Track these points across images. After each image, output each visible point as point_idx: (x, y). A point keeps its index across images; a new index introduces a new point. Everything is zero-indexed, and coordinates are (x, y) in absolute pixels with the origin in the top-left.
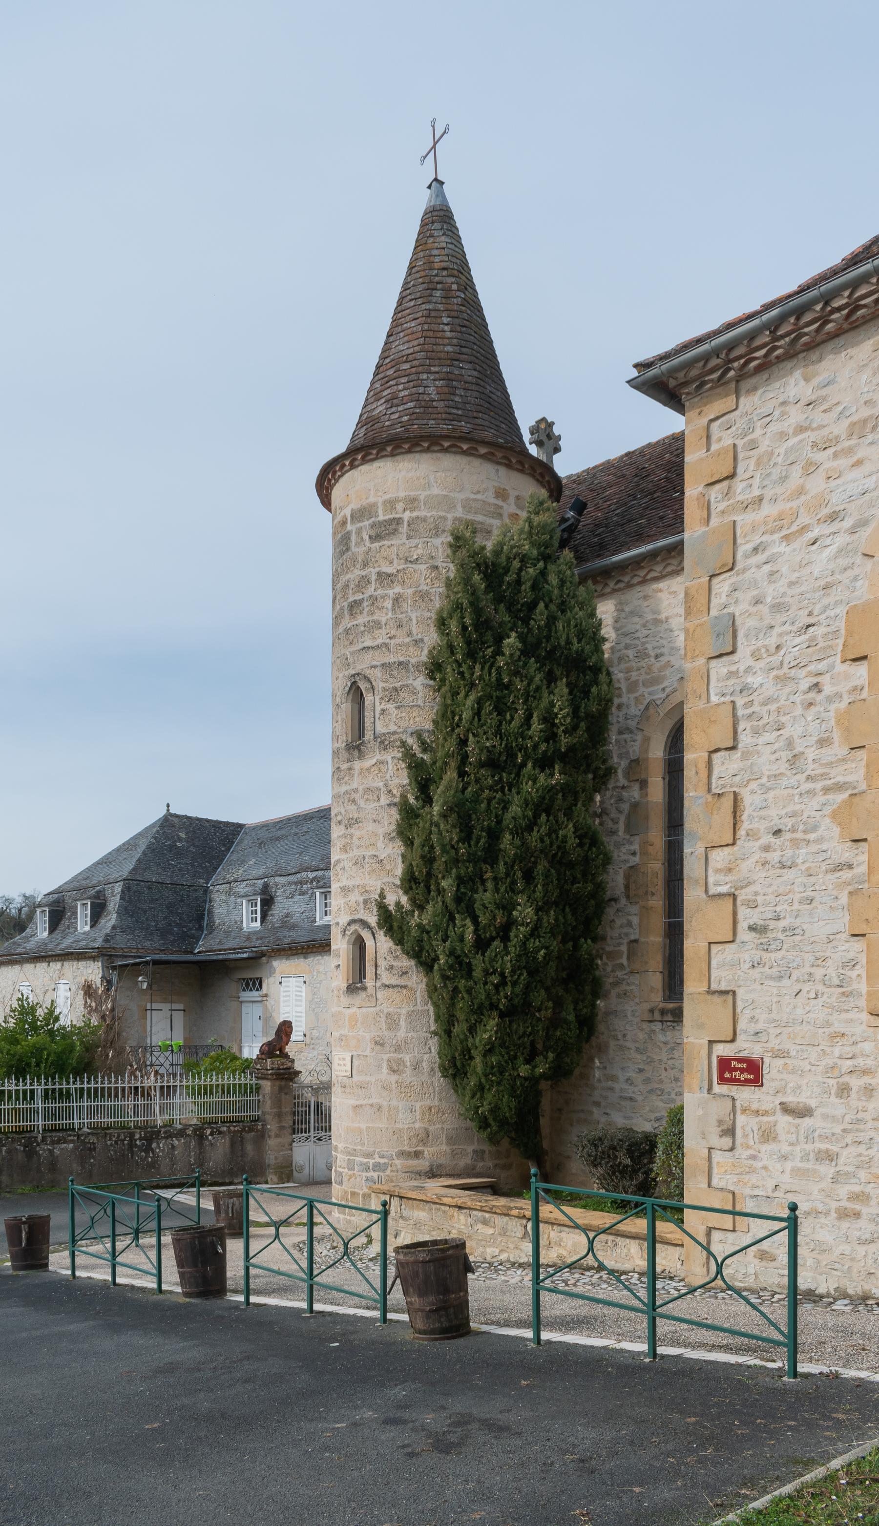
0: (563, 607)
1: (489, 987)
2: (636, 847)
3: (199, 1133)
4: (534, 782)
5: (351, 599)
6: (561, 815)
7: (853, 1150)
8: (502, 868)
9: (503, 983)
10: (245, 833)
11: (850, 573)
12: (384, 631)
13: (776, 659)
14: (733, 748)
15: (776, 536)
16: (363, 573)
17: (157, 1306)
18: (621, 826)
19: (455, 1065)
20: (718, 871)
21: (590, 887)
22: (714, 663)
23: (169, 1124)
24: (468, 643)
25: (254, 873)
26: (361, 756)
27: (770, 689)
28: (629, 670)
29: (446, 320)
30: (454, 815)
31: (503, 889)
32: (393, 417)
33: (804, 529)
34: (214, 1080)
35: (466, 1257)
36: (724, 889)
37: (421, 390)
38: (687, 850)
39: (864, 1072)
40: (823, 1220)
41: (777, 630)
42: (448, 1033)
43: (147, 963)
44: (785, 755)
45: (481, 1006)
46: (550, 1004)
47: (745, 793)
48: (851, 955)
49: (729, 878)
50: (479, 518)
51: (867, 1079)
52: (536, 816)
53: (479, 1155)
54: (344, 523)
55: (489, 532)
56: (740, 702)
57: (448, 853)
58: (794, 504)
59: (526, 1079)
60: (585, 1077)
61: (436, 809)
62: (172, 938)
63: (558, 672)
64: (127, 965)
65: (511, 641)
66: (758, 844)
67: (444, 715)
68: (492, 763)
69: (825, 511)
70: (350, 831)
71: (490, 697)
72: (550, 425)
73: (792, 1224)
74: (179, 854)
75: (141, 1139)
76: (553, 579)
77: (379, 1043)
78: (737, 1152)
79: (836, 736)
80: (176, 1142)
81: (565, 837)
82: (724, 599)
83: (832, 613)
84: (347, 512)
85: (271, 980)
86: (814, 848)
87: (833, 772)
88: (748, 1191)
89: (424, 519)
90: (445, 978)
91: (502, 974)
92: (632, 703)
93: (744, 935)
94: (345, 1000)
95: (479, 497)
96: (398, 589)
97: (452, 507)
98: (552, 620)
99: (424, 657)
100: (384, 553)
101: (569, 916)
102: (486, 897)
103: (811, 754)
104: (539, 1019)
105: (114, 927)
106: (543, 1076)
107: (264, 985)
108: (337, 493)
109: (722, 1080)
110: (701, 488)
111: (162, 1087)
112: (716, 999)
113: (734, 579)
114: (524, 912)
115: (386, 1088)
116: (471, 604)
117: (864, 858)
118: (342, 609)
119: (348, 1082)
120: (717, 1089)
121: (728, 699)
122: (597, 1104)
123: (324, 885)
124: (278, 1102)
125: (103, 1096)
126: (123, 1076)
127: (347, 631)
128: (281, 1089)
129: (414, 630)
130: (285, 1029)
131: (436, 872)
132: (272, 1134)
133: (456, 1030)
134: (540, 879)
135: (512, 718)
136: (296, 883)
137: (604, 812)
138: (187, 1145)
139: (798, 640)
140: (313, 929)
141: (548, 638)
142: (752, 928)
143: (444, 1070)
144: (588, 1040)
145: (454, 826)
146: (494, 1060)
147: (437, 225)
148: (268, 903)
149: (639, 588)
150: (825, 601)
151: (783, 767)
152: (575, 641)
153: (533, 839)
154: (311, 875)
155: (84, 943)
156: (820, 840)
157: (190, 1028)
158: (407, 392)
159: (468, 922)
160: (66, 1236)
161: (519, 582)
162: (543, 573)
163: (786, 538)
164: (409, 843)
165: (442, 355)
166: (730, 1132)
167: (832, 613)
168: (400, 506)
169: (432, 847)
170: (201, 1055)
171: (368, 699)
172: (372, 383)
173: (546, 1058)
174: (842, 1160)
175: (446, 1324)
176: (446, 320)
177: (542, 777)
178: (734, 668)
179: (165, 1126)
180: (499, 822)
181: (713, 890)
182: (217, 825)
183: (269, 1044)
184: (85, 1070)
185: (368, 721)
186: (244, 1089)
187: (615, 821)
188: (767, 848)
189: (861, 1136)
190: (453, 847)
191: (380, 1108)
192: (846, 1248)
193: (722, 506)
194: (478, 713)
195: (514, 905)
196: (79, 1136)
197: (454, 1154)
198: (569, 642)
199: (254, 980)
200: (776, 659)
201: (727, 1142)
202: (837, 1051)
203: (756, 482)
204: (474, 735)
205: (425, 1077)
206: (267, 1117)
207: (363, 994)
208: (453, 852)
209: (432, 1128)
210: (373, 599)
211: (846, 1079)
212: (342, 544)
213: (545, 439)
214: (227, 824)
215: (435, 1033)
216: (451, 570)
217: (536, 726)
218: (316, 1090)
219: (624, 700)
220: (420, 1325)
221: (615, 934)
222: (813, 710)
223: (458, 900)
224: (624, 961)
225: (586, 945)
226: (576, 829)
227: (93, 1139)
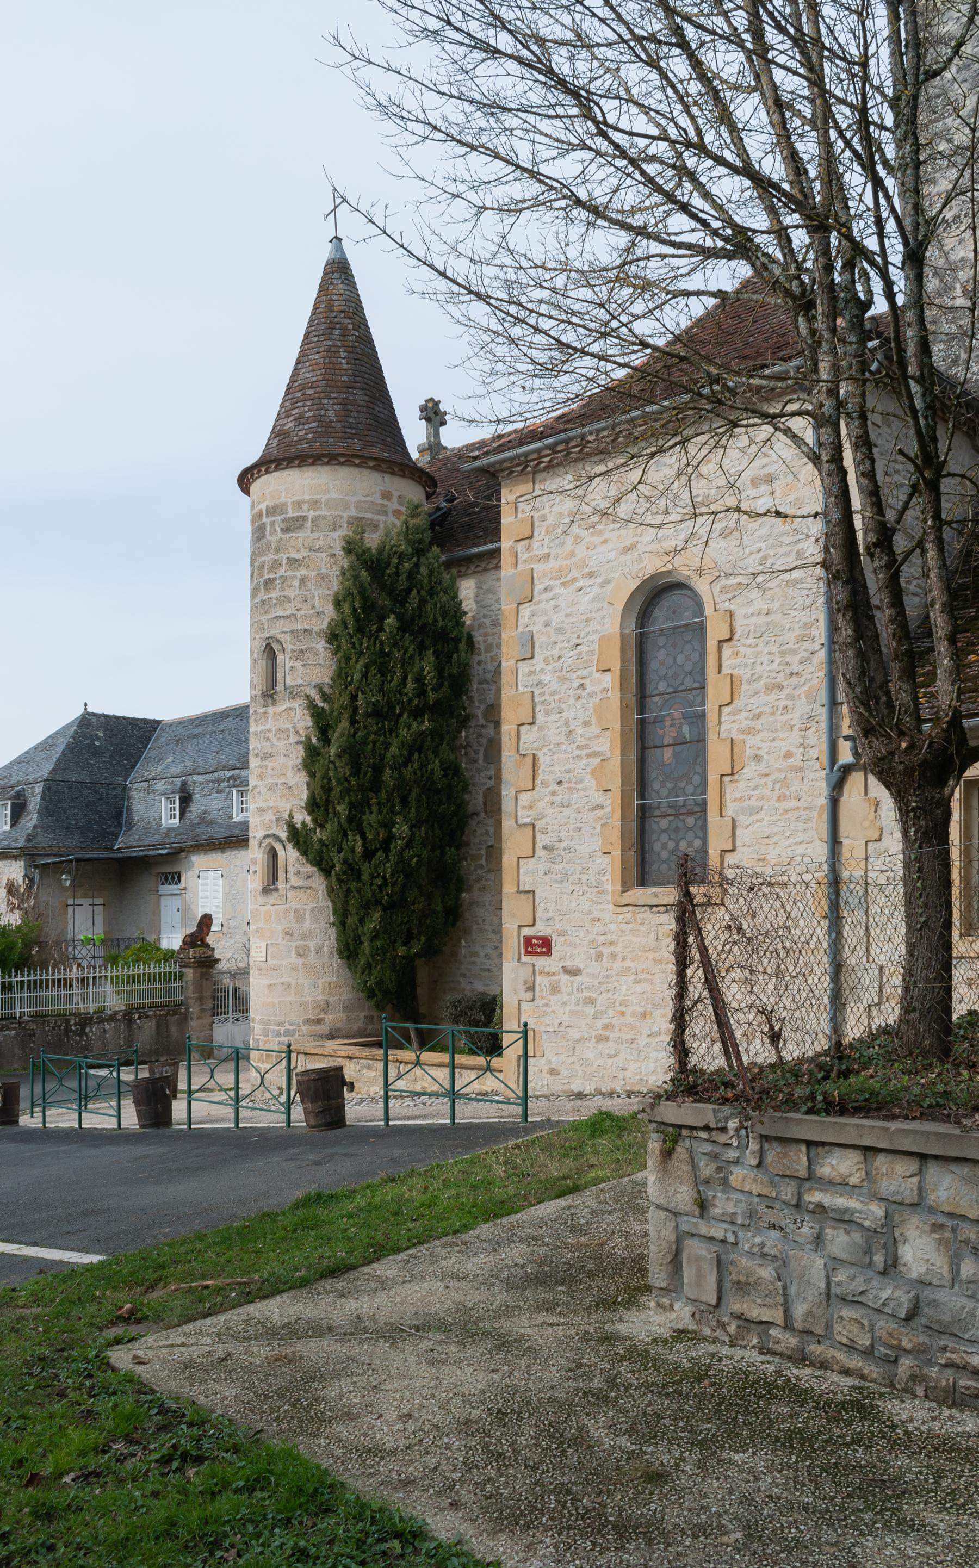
0: (432, 592)
1: (375, 887)
2: (491, 773)
3: (126, 1018)
4: (409, 729)
5: (266, 577)
6: (430, 753)
7: (605, 996)
8: (384, 795)
9: (385, 883)
10: (162, 729)
11: (600, 613)
12: (292, 605)
13: (559, 665)
14: (533, 723)
15: (558, 582)
16: (276, 557)
17: (119, 1136)
18: (481, 756)
19: (349, 949)
20: (524, 808)
21: (453, 808)
22: (520, 664)
23: (101, 1010)
24: (357, 620)
25: (172, 771)
26: (274, 703)
27: (555, 685)
28: (486, 635)
29: (343, 355)
30: (347, 756)
31: (384, 812)
32: (301, 433)
33: (574, 580)
34: (141, 969)
35: (343, 1077)
36: (527, 820)
37: (323, 412)
38: (504, 793)
39: (611, 944)
40: (588, 1044)
41: (559, 645)
42: (343, 924)
43: (70, 861)
44: (564, 730)
45: (368, 902)
46: (422, 899)
47: (540, 755)
48: (603, 866)
49: (530, 813)
50: (369, 516)
51: (612, 948)
52: (411, 754)
53: (370, 1019)
54: (260, 515)
55: (376, 526)
56: (537, 692)
57: (342, 784)
58: (569, 562)
59: (403, 957)
60: (454, 954)
61: (333, 751)
62: (91, 836)
63: (428, 642)
64: (49, 864)
65: (391, 620)
66: (548, 790)
67: (339, 676)
68: (376, 713)
69: (586, 570)
70: (265, 763)
71: (374, 663)
72: (437, 404)
73: (525, 1033)
74: (98, 752)
75: (75, 1024)
76: (424, 571)
77: (289, 934)
78: (536, 1002)
79: (594, 720)
80: (107, 1027)
81: (433, 770)
82: (526, 620)
83: (590, 638)
84: (263, 507)
85: (190, 874)
86: (581, 794)
87: (592, 745)
88: (543, 1029)
89: (324, 517)
90: (340, 881)
91: (384, 877)
92: (489, 660)
93: (540, 852)
94: (261, 899)
95: (368, 499)
96: (304, 572)
97: (347, 507)
98: (423, 602)
99: (325, 625)
100: (293, 543)
101: (437, 831)
102: (371, 818)
103: (579, 731)
104: (413, 911)
105: (35, 827)
106: (417, 955)
107: (183, 879)
108: (254, 488)
109: (527, 952)
110: (511, 543)
111: (94, 978)
112: (523, 896)
113: (532, 608)
114: (402, 829)
115: (294, 969)
116: (359, 593)
117: (609, 802)
118: (259, 583)
119: (263, 965)
120: (525, 959)
121: (529, 689)
122: (464, 975)
123: (242, 785)
124: (199, 988)
125: (41, 987)
126: (47, 970)
127: (263, 602)
128: (203, 976)
129: (317, 605)
130: (206, 921)
131: (332, 798)
132: (195, 1016)
133: (349, 921)
134: (413, 803)
135: (392, 679)
136: (213, 782)
137: (468, 745)
138: (117, 1029)
139: (571, 654)
140: (231, 825)
141: (420, 616)
142: (545, 848)
143: (340, 952)
144: (454, 925)
145: (347, 764)
146: (378, 944)
147: (336, 275)
148: (186, 800)
149: (493, 572)
150: (587, 630)
151: (563, 738)
152: (440, 619)
153: (408, 772)
154: (229, 774)
155: (6, 843)
156: (584, 789)
157: (110, 923)
158: (311, 414)
159: (358, 837)
160: (28, 1104)
161: (397, 573)
162: (417, 565)
163: (563, 584)
164: (312, 775)
165: (340, 384)
166: (532, 988)
167: (590, 638)
168: (305, 507)
169: (330, 779)
170: (122, 947)
171: (280, 658)
172: (284, 402)
173: (419, 940)
174: (599, 1003)
175: (329, 1120)
176: (343, 355)
177: (415, 724)
178: (533, 669)
179: (95, 1012)
180: (382, 759)
181: (521, 821)
182: (134, 723)
183: (192, 935)
184: (24, 965)
185: (280, 675)
186: (168, 977)
187: (476, 752)
188: (553, 793)
189: (611, 986)
190: (346, 779)
191: (289, 985)
192: (601, 1062)
193: (526, 556)
194: (365, 675)
195: (393, 824)
196: (20, 1023)
197: (349, 1019)
198: (435, 620)
199: (173, 874)
200: (559, 665)
201: (529, 995)
202: (595, 931)
203: (546, 543)
204: (363, 693)
205: (326, 959)
206: (190, 1001)
207: (275, 894)
208: (346, 784)
209: (331, 1000)
210: (284, 579)
211: (601, 948)
212: (259, 532)
213: (432, 415)
214: (144, 720)
215: (333, 924)
216: (344, 561)
217: (410, 685)
218: (233, 976)
219: (483, 657)
220: (312, 1122)
221: (477, 841)
222: (581, 701)
223: (350, 820)
224: (483, 862)
225: (450, 852)
226: (441, 763)
227: (33, 1026)
